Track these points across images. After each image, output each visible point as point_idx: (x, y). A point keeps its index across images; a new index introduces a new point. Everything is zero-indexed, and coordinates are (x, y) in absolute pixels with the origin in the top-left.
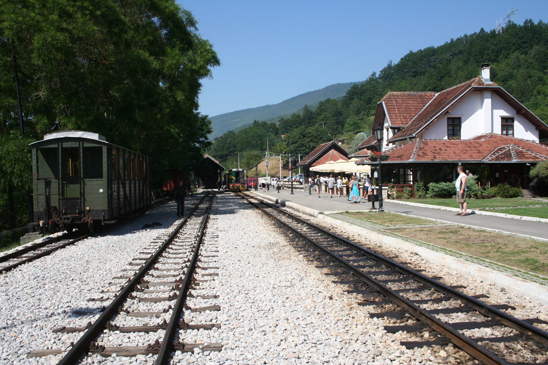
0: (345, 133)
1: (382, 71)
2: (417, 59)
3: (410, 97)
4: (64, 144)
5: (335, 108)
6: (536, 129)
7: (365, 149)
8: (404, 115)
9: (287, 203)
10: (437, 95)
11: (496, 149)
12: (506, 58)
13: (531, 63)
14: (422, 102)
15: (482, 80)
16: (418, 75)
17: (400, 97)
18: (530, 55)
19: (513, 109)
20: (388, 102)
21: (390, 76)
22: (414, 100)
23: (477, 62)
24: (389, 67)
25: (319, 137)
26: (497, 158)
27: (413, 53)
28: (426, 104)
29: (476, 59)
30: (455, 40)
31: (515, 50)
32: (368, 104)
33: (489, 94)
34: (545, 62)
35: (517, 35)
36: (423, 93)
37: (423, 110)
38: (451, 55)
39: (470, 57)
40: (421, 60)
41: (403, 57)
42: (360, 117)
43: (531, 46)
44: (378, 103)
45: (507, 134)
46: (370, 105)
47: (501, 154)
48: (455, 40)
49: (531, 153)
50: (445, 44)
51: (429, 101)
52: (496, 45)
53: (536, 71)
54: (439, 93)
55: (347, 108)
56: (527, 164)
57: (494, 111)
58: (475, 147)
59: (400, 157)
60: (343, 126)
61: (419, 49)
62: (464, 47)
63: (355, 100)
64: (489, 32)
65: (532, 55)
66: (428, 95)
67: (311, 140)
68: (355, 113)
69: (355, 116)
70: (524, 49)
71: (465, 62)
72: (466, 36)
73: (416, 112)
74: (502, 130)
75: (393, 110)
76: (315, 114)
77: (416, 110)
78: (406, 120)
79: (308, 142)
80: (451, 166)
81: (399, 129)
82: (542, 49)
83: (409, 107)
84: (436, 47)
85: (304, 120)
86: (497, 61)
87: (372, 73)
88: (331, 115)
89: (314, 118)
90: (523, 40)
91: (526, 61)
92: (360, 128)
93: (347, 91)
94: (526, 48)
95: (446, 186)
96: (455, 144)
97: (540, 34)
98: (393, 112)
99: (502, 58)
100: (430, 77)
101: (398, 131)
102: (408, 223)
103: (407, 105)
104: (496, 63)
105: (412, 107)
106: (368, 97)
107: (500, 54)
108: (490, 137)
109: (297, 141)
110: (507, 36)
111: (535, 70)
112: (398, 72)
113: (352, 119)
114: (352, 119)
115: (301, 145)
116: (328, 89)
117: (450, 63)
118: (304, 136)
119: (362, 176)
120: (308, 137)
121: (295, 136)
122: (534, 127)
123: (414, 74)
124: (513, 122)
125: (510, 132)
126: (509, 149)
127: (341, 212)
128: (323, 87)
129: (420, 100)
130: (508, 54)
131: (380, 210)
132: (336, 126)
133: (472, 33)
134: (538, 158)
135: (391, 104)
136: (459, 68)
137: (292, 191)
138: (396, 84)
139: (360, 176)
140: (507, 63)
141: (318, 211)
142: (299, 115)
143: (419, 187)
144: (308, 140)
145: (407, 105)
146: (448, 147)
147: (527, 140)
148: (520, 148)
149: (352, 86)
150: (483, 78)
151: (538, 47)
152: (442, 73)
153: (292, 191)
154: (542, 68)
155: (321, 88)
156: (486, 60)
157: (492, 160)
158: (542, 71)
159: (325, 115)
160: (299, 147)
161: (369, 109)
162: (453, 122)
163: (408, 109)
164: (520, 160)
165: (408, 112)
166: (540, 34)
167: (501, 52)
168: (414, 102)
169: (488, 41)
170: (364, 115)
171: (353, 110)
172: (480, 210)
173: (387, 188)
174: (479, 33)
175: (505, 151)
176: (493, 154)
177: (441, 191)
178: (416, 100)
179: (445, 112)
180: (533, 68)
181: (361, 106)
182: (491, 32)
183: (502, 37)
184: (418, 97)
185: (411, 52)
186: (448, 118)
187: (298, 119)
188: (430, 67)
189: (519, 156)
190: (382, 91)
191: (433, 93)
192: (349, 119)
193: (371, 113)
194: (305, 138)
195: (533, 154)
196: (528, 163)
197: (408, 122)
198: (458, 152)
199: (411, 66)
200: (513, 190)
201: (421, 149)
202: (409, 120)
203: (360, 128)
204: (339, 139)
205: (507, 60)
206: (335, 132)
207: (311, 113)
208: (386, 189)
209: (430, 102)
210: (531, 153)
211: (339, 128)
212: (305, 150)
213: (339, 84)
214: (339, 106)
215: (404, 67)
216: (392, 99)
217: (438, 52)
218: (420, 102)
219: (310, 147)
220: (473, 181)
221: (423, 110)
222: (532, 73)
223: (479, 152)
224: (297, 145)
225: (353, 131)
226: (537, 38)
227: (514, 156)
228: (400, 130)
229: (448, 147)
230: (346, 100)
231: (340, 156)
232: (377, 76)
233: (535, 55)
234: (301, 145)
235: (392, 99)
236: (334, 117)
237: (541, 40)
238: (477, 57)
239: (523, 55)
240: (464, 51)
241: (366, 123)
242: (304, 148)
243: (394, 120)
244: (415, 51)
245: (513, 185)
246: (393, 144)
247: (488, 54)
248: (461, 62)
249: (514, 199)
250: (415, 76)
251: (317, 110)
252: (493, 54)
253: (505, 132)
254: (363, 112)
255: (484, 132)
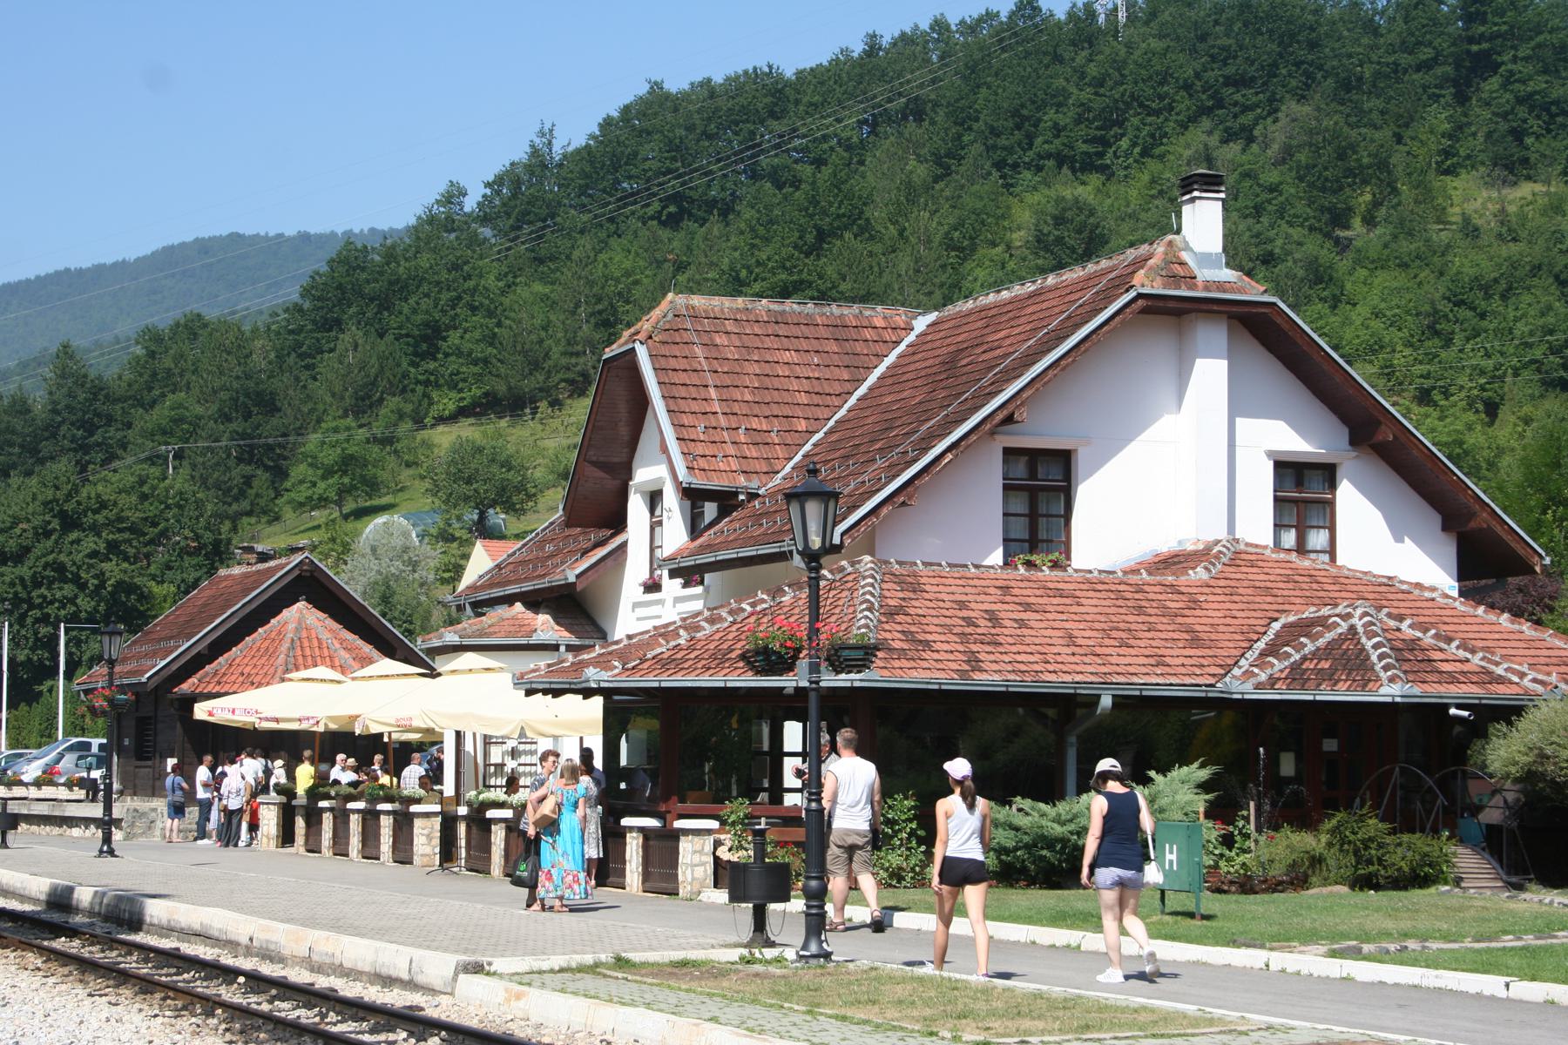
0: (289, 514)
1: (499, 181)
2: (690, 128)
3: (782, 330)
4: (786, 749)
5: (238, 371)
6: (1446, 527)
7: (519, 606)
8: (755, 423)
9: (155, 911)
10: (921, 323)
11: (1276, 626)
12: (1145, 153)
13: (1273, 189)
14: (847, 360)
15: (1185, 256)
16: (690, 215)
17: (730, 326)
18: (1267, 146)
19: (1334, 419)
20: (665, 350)
21: (544, 212)
22: (805, 345)
23: (999, 165)
24: (538, 162)
25: (153, 532)
26: (1296, 675)
27: (667, 96)
28: (870, 369)
29: (995, 147)
30: (886, 41)
31: (1193, 119)
32: (423, 356)
33: (1214, 334)
34: (1341, 188)
35: (1203, 38)
36: (850, 312)
37: (852, 401)
38: (865, 122)
39: (966, 139)
40: (710, 137)
41: (615, 114)
42: (378, 429)
43: (1271, 100)
44: (609, 353)
45: (1301, 548)
46: (432, 365)
47: (1314, 654)
48: (886, 41)
49: (1462, 654)
50: (835, 62)
51: (881, 357)
52: (1099, 83)
53: (1296, 233)
54: (932, 317)
55: (304, 375)
56: (1453, 711)
57: (1239, 420)
58: (1166, 612)
59: (664, 663)
60: (280, 473)
61: (698, 78)
62: (933, 81)
63: (352, 333)
64: (1061, 15)
65: (1276, 147)
66: (879, 322)
67: (113, 547)
68: (348, 401)
69: (350, 421)
70: (1235, 116)
71: (938, 160)
72: (940, 25)
73: (820, 413)
74: (1278, 526)
75: (694, 392)
76: (119, 400)
77: (817, 399)
78: (765, 452)
79: (94, 554)
80: (1051, 712)
81: (727, 501)
82: (1328, 123)
83: (776, 383)
84: (789, 73)
85: (51, 430)
86: (1103, 169)
87: (442, 187)
88: (214, 408)
89: (110, 420)
90: (1230, 70)
91: (1246, 175)
92: (373, 486)
93: (305, 281)
94: (1246, 109)
95: (1058, 820)
96: (1061, 594)
97: (1313, 45)
98: (695, 407)
99: (1127, 155)
100: (761, 231)
101: (724, 512)
102: (1087, 1027)
103: (767, 369)
104: (1095, 179)
105: (795, 384)
106: (419, 318)
107: (1116, 130)
108: (1233, 563)
109: (27, 550)
110: (1155, 44)
111: (1290, 224)
112: (583, 191)
113: (334, 437)
114: (334, 437)
115: (49, 573)
116: (170, 259)
117: (861, 163)
118: (70, 522)
119: (496, 755)
120: (96, 529)
121: (16, 521)
122: (1436, 520)
123: (672, 209)
124: (1333, 486)
125: (1318, 539)
126: (1352, 628)
127: (588, 959)
128: (146, 249)
129: (833, 347)
130: (1158, 137)
131: (814, 948)
132: (238, 472)
133: (974, 11)
134: (1501, 680)
135: (683, 364)
136: (911, 193)
137: (107, 839)
138: (576, 254)
139: (486, 754)
140: (1153, 181)
141: (449, 961)
142: (24, 402)
143: (890, 823)
144: (90, 543)
145: (767, 369)
146: (1028, 607)
147: (1418, 585)
148: (1404, 626)
149: (331, 252)
150: (1187, 248)
151: (1307, 109)
152: (825, 213)
153: (107, 839)
154: (1327, 216)
155: (131, 255)
156: (1049, 156)
157: (1272, 682)
158: (1328, 235)
159: (180, 406)
160: (38, 585)
161: (427, 383)
162: (1033, 475)
163: (776, 396)
164: (1417, 690)
165: (776, 410)
166: (1313, 45)
167: (1120, 124)
168: (807, 358)
169: (1058, 59)
170: (401, 416)
171: (338, 388)
172: (1333, 954)
173: (714, 824)
174: (1012, 15)
175: (1329, 636)
176: (1272, 650)
177: (1027, 847)
178: (815, 345)
179: (1000, 416)
180: (1281, 213)
181: (382, 369)
182: (1071, 15)
183: (1129, 46)
184: (823, 332)
185: (656, 86)
186: (1008, 452)
187: (18, 423)
188: (755, 176)
189: (1406, 667)
190: (503, 293)
191: (899, 315)
192: (314, 438)
193: (434, 412)
194: (74, 535)
195: (1476, 659)
196: (1459, 707)
197: (777, 465)
198: (1086, 637)
199: (655, 165)
200: (1404, 850)
201: (891, 614)
202: (780, 452)
203: (373, 486)
204: (259, 548)
205: (1153, 165)
206: (235, 507)
207: (98, 390)
208: (709, 832)
209: (890, 359)
210: (1462, 654)
211: (255, 483)
212: (72, 601)
213: (235, 238)
214: (258, 361)
215: (616, 168)
216: (686, 336)
217: (797, 102)
218: (836, 359)
219: (102, 585)
220: (1190, 797)
221: (852, 401)
222: (1279, 242)
223: (1195, 641)
224: (24, 571)
225: (339, 503)
226: (1298, 64)
227: (1386, 668)
228: (735, 507)
229: (1028, 607)
230: (300, 330)
231: (342, 641)
232: (470, 204)
233: (1288, 152)
234: (49, 573)
235: (686, 336)
236: (228, 419)
237: (1319, 76)
238: (1003, 141)
239: (1235, 148)
240: (936, 105)
241: (408, 465)
242: (68, 590)
243: (700, 449)
244: (676, 83)
245: (1405, 822)
246: (685, 585)
247: (1058, 130)
248: (920, 159)
249: (1416, 895)
250: (673, 222)
251: (128, 376)
252: (1082, 131)
253: (1289, 538)
254: (393, 402)
255: (1193, 535)
